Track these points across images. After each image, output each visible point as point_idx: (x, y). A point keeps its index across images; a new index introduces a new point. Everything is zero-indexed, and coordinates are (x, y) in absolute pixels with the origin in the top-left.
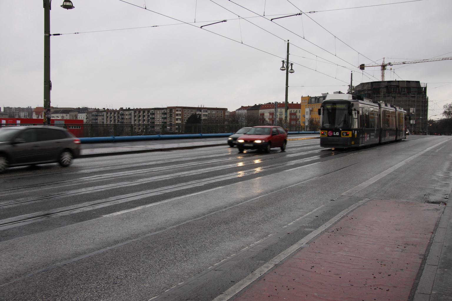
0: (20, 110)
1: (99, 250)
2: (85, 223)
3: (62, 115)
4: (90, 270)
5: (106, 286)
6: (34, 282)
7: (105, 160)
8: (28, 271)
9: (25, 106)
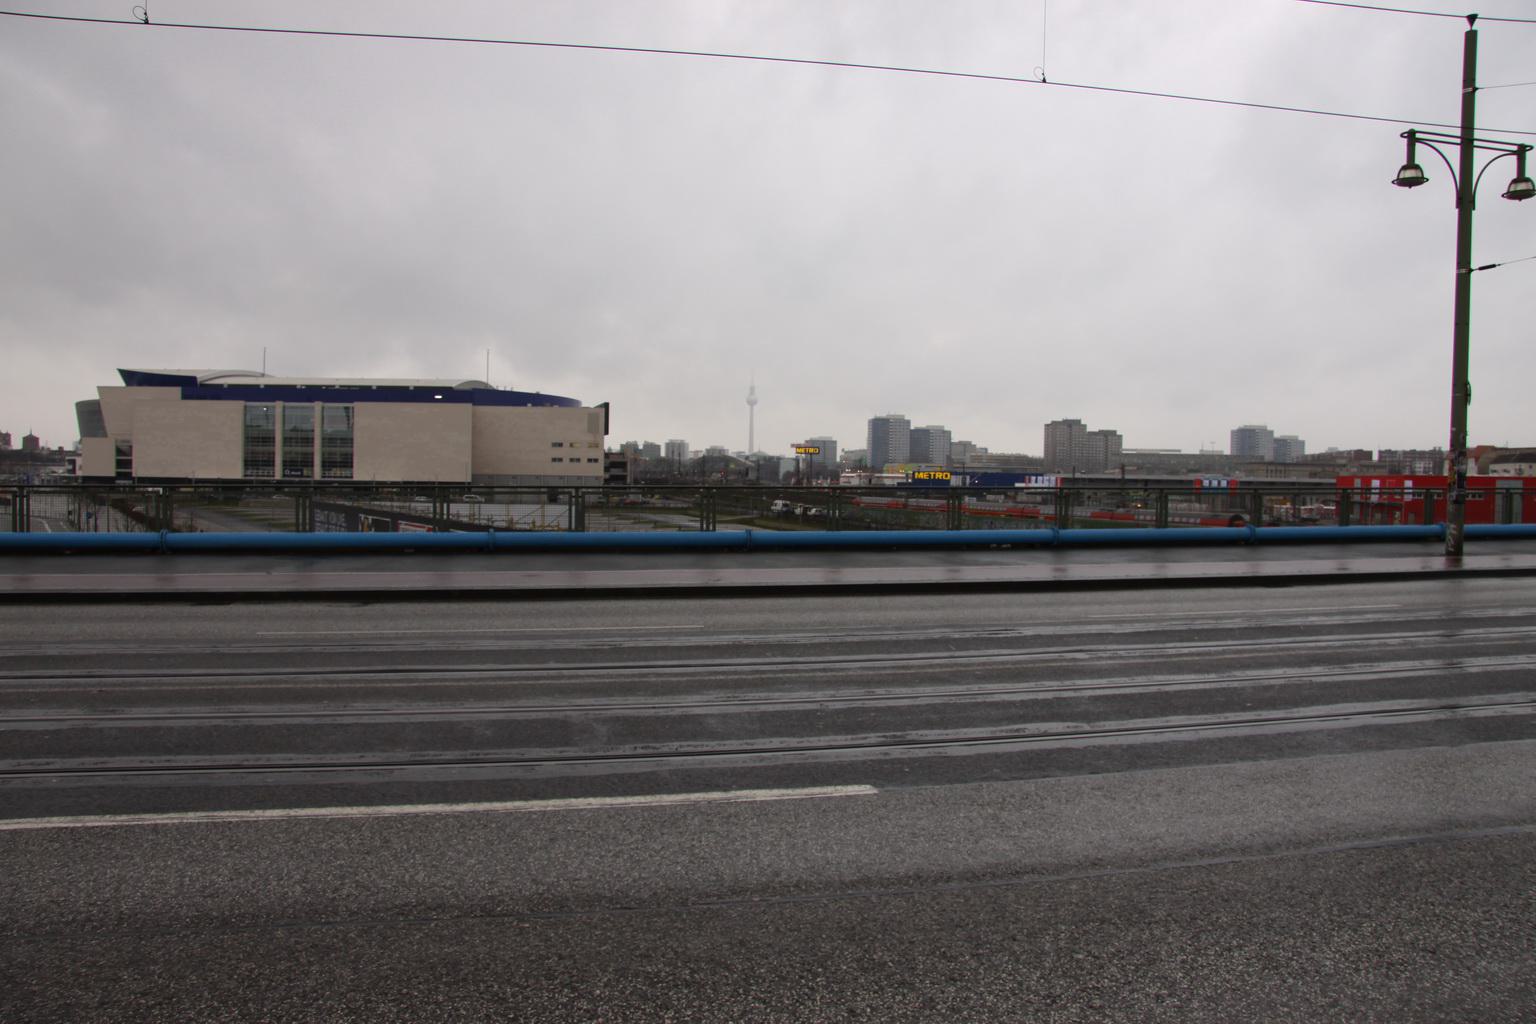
0: (1414, 455)
1: (1519, 824)
2: (1498, 747)
3: (1517, 466)
4: (1475, 873)
5: (1511, 928)
6: (1323, 868)
7: (1512, 588)
8: (1318, 840)
9: (1428, 447)
